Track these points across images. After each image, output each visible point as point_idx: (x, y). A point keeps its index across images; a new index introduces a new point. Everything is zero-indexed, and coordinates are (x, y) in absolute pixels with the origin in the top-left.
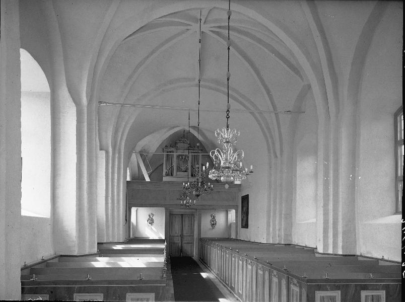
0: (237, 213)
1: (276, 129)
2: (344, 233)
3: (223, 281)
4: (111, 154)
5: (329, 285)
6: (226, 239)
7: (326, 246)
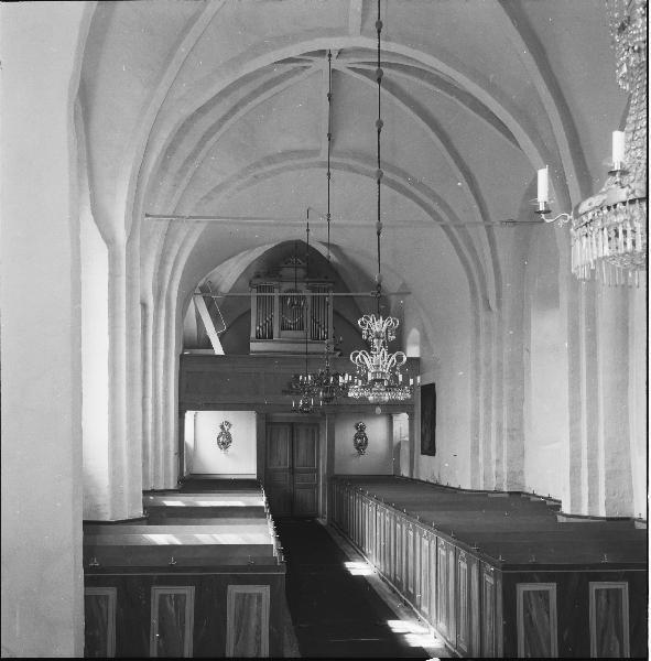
0: (411, 420)
1: (487, 250)
2: (609, 476)
3: (390, 579)
7: (575, 500)
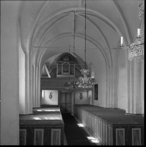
4: (34, 68)
5: (121, 126)
6: (87, 106)
7: (129, 110)
